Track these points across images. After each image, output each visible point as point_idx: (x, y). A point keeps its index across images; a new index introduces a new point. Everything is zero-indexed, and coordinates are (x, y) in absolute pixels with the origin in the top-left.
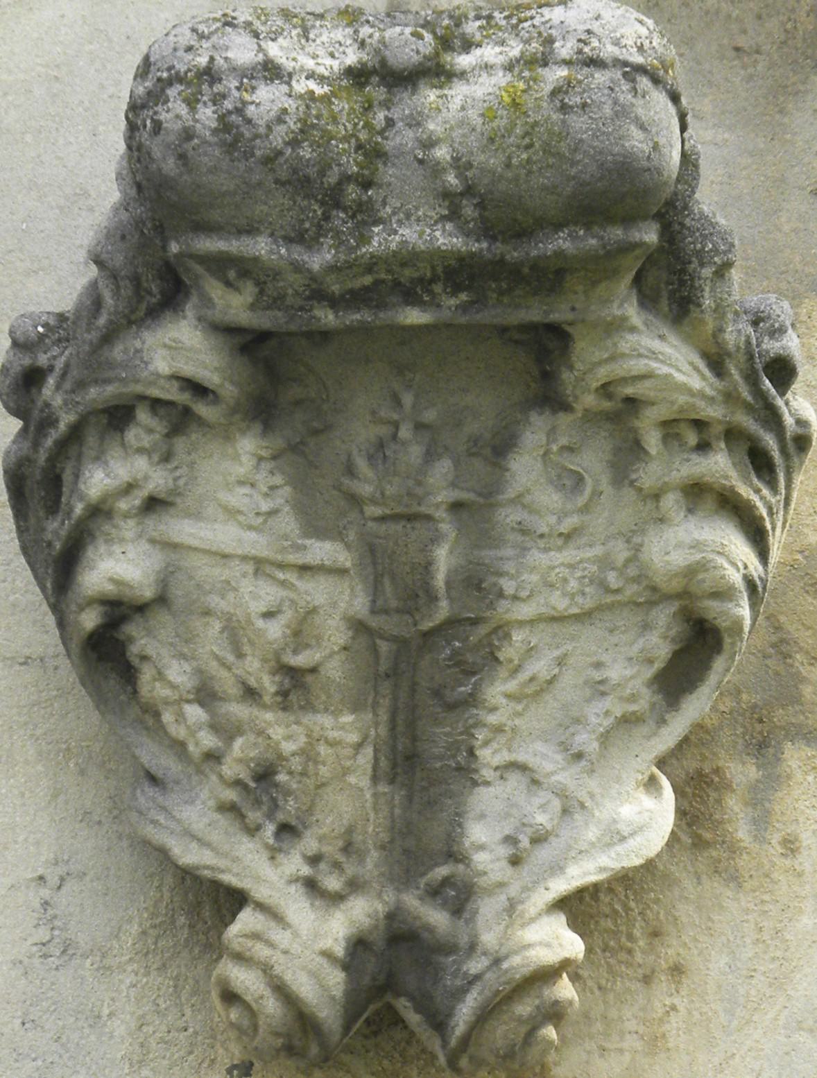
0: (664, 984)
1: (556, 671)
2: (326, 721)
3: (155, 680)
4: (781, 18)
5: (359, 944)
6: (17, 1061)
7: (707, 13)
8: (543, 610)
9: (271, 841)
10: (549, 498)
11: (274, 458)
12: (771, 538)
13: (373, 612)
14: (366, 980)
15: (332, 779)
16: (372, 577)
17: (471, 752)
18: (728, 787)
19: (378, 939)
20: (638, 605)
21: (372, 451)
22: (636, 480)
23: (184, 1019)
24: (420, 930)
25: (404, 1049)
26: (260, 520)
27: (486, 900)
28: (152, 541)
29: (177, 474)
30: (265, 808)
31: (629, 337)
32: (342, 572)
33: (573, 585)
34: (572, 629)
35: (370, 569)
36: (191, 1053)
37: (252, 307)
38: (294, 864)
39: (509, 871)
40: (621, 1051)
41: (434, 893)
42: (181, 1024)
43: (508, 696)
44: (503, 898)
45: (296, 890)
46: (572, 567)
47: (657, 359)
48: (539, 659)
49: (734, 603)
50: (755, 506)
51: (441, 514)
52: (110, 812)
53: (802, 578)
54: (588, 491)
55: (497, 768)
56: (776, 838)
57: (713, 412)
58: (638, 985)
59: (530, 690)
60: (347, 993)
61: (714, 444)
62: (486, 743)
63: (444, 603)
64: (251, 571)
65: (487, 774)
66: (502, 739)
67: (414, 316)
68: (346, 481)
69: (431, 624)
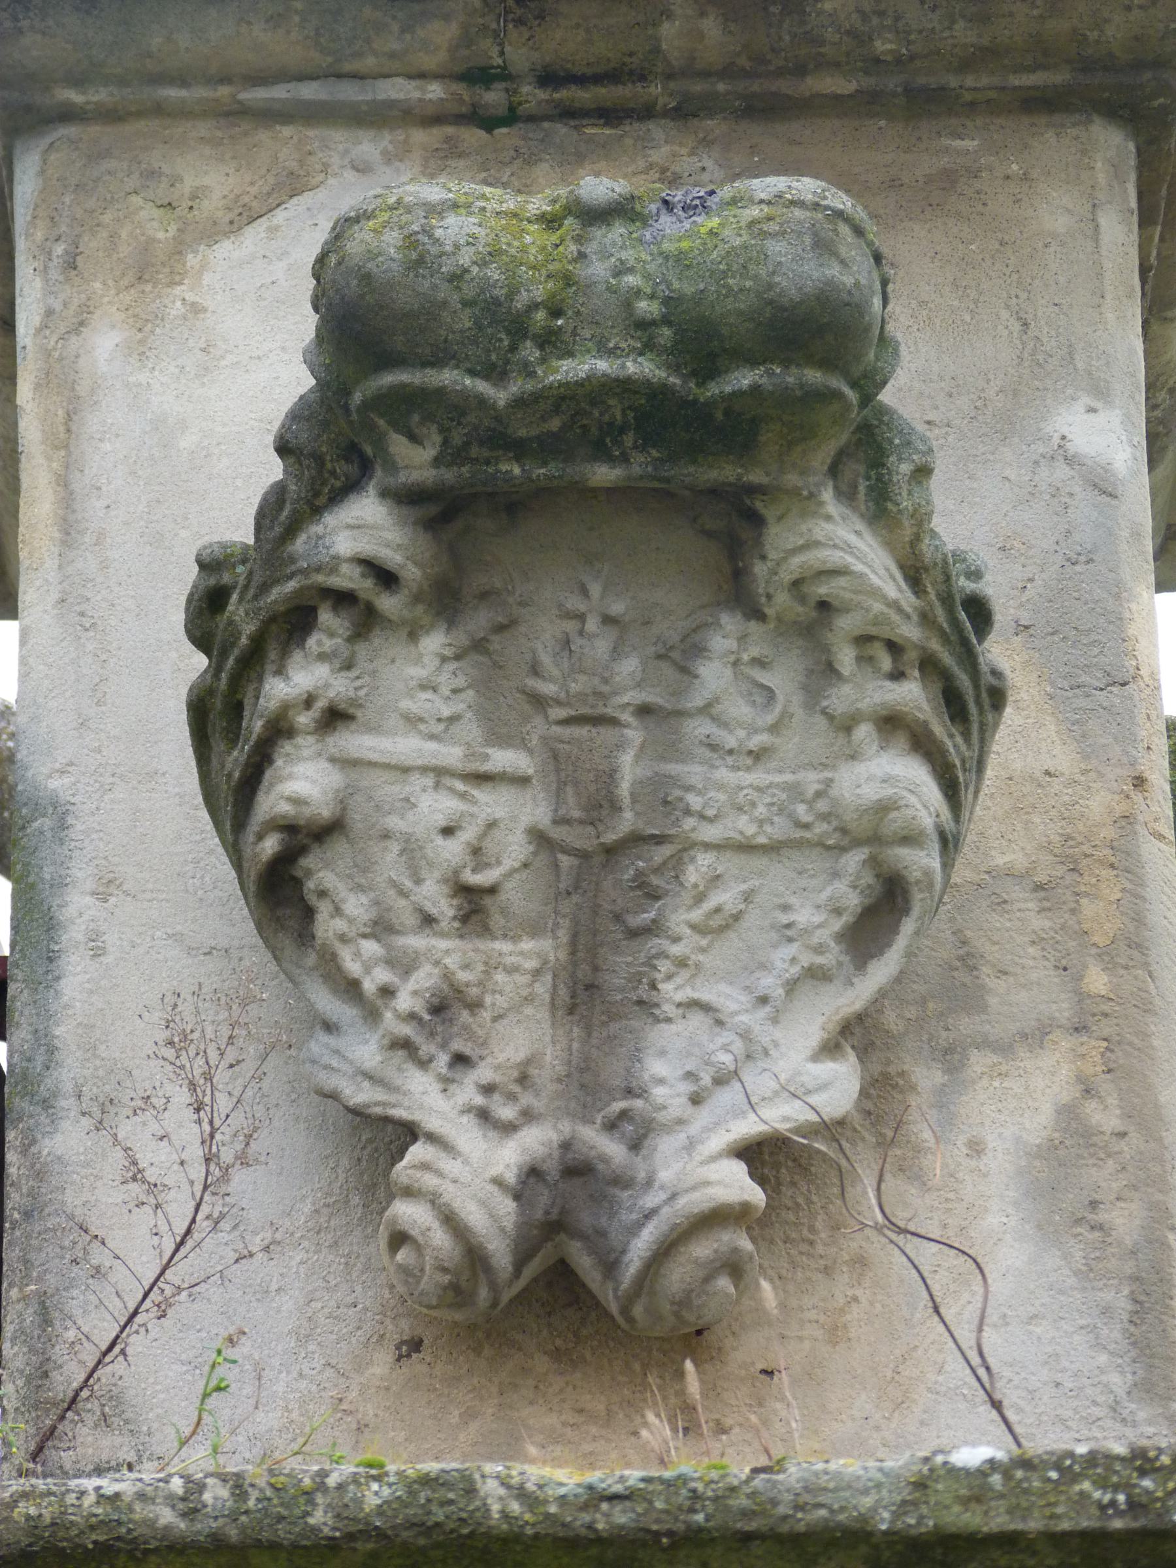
0: (846, 1276)
1: (742, 906)
2: (501, 946)
3: (332, 917)
4: (972, 396)
5: (533, 1173)
6: (181, 1331)
7: (900, 390)
8: (732, 834)
9: (444, 1071)
10: (739, 709)
11: (457, 657)
12: (963, 792)
13: (555, 822)
14: (539, 1215)
15: (509, 1010)
16: (554, 786)
17: (653, 986)
18: (913, 1088)
19: (552, 1168)
20: (828, 848)
21: (557, 649)
22: (827, 707)
23: (354, 1295)
24: (595, 1161)
25: (579, 1329)
26: (441, 727)
27: (666, 1138)
28: (333, 760)
29: (358, 683)
30: (439, 1039)
31: (824, 524)
32: (522, 781)
33: (761, 810)
34: (758, 862)
35: (553, 777)
36: (359, 1328)
37: (437, 462)
38: (467, 1092)
39: (690, 1110)
40: (801, 1339)
41: (611, 1126)
42: (350, 1299)
43: (693, 927)
44: (683, 1136)
45: (468, 1120)
46: (759, 790)
47: (851, 553)
48: (724, 891)
49: (925, 852)
50: (948, 751)
51: (626, 717)
52: (288, 1095)
53: (990, 896)
54: (778, 709)
55: (679, 1005)
56: (961, 1141)
57: (910, 632)
58: (820, 1275)
59: (715, 922)
60: (519, 1226)
61: (908, 671)
62: (669, 977)
63: (628, 815)
64: (431, 784)
65: (669, 1009)
66: (684, 974)
67: (604, 474)
68: (532, 683)
69: (614, 837)
